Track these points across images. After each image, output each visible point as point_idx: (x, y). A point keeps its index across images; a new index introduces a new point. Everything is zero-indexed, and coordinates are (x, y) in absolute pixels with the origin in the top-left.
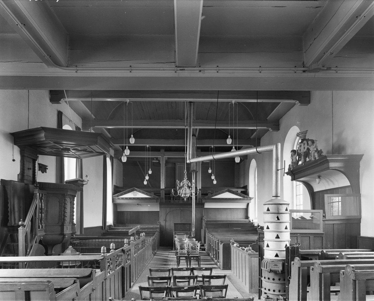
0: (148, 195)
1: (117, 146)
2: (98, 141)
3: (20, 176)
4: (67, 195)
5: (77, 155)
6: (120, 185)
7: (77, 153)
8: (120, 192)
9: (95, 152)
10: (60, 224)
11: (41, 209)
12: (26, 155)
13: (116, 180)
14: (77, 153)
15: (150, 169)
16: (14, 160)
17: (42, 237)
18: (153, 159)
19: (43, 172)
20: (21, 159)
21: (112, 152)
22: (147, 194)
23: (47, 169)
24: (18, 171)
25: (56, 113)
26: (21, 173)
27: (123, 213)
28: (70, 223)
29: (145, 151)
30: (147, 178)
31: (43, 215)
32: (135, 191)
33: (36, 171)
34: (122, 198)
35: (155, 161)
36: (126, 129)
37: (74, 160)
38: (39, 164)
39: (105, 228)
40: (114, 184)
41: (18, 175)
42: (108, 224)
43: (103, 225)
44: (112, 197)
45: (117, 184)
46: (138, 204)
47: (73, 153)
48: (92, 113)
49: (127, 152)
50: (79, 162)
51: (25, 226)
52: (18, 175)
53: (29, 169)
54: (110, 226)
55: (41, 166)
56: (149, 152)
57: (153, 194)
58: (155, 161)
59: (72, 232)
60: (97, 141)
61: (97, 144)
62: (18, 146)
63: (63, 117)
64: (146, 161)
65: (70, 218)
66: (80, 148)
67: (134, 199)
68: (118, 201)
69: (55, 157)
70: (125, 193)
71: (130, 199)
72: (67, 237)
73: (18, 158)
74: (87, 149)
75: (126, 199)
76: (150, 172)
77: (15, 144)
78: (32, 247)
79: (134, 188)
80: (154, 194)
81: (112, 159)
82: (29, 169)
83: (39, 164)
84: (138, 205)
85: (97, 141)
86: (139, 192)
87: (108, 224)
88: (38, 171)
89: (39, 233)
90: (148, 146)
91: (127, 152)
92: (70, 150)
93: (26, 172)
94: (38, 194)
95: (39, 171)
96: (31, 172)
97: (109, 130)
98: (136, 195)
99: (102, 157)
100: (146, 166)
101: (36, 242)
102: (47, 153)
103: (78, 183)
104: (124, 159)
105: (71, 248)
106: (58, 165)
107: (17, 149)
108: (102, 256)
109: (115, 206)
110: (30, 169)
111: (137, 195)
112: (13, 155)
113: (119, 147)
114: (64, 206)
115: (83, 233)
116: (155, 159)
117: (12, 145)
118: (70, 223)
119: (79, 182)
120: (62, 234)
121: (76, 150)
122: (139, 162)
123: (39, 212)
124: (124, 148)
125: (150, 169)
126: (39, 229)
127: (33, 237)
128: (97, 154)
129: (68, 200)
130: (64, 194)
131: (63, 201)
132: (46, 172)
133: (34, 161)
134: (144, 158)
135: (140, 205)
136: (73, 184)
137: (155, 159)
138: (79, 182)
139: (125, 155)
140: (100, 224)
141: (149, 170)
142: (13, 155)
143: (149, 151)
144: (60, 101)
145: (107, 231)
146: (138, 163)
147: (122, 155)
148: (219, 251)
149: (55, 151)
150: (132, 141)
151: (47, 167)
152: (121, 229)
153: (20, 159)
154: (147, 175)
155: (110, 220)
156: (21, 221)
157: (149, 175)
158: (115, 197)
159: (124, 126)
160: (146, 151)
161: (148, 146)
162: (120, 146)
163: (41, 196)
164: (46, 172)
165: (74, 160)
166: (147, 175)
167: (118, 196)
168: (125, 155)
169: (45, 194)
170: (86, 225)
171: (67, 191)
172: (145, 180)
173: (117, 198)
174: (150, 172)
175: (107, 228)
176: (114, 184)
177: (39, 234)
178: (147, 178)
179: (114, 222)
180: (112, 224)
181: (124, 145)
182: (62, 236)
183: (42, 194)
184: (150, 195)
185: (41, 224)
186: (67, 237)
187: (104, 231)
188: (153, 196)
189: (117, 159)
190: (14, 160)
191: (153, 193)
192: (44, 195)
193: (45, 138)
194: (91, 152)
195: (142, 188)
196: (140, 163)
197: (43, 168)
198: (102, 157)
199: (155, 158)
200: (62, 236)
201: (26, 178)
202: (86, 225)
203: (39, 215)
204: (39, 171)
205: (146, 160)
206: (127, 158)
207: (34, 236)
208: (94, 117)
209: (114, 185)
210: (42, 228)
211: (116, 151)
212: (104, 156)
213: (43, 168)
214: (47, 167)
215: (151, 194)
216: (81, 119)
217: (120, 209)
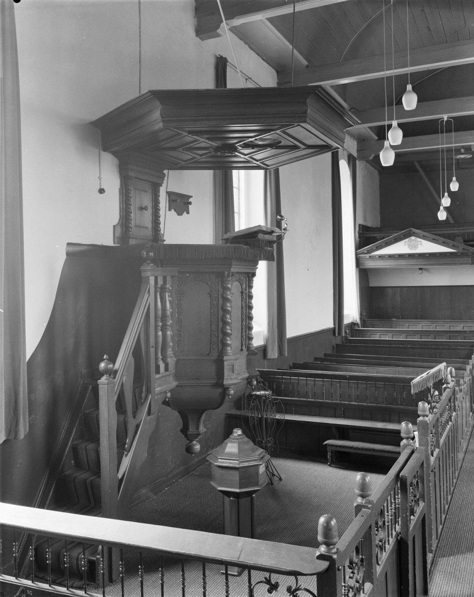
0: (448, 247)
1: (363, 128)
2: (309, 111)
3: (119, 230)
4: (228, 276)
5: (257, 161)
6: (373, 221)
7: (258, 156)
8: (374, 240)
9: (302, 146)
10: (215, 355)
11: (164, 316)
12: (131, 174)
13: (365, 211)
14: (258, 156)
15: (454, 179)
16: (102, 191)
17: (169, 395)
18: (458, 151)
19: (180, 214)
20: (121, 185)
21: (351, 145)
22: (444, 244)
23: (190, 203)
24: (114, 216)
25: (212, 62)
26: (122, 223)
27: (382, 290)
28: (242, 350)
29: (439, 133)
30: (446, 202)
31: (169, 333)
32: (413, 238)
33: (162, 213)
34: (381, 257)
35: (462, 156)
36: (389, 78)
37: (258, 175)
38: (169, 194)
39: (340, 333)
40: (360, 221)
41: (114, 226)
42: (347, 321)
43: (334, 324)
44: (356, 254)
45: (365, 220)
46: (421, 269)
47: (246, 157)
48: (295, 46)
49: (395, 137)
50: (270, 178)
51: (116, 372)
52: (114, 226)
53: (141, 209)
54: (353, 325)
55: (174, 198)
56: (449, 134)
57: (462, 240)
58: (462, 156)
59: (248, 375)
60: (307, 111)
61: (305, 122)
62: (115, 154)
63: (229, 70)
64: (443, 160)
65: (242, 337)
66: (261, 139)
67: (411, 256)
68: (370, 264)
69: (211, 172)
70: (388, 244)
71: (401, 256)
72: (232, 392)
73: (112, 182)
74: (280, 142)
75: (391, 257)
76: (454, 186)
77: (105, 150)
78: (138, 426)
79: (411, 230)
80: (465, 241)
81: (351, 160)
82: (141, 209)
83: (169, 194)
84: (420, 271)
85: (306, 112)
86: (424, 238)
87: (347, 321)
88: (168, 212)
89: (160, 385)
90: (445, 117)
91: (395, 137)
92: (235, 149)
93: (135, 217)
94: (152, 280)
95: (170, 210)
96: (148, 215)
97: (342, 89)
98: (416, 247)
99: (328, 156)
100: (443, 170)
101: (149, 413)
102: (184, 163)
103: (259, 240)
104: (387, 159)
105: (239, 435)
106: (217, 190)
107: (109, 163)
108: (321, 557)
109: (364, 274)
110: (146, 208)
111: (419, 246)
112: (100, 178)
113: (368, 129)
114: (223, 305)
115: (286, 355)
116: (463, 151)
117: (97, 151)
118: (242, 350)
119: (260, 236)
120: (219, 383)
121: (253, 148)
122: (419, 162)
123: (156, 326)
124: (382, 133)
125: (454, 179)
126: (157, 376)
127: (141, 398)
128: (311, 150)
129: (234, 288)
130: (223, 273)
131: (220, 293)
132: (188, 213)
133: (155, 189)
134: (436, 151)
135: (426, 270)
136: (247, 244)
137: (463, 151)
138: (260, 236)
139: (390, 145)
140: (328, 323)
141: (450, 181)
142: (100, 178)
143: (449, 131)
144: (218, 29)
145: (346, 338)
146: (417, 165)
147: (382, 147)
148: (300, 112)
149: (201, 155)
150: (410, 101)
151: (190, 200)
152: (380, 334)
153: (118, 186)
154: (446, 194)
155: (352, 311)
156: (104, 360)
157: (452, 195)
158: (363, 253)
159: (383, 70)
160: (442, 132)
161: (445, 117)
162: (370, 128)
163: (160, 282)
164: (188, 213)
165: (258, 175)
166: (446, 194)
167: (369, 252)
168: (390, 145)
169: (172, 277)
170: (291, 332)
171: (231, 265)
172: (441, 208)
173: (367, 256)
174: (454, 186)
175: (346, 332)
176: (360, 221)
177: (158, 389)
178: (446, 202)
179: (361, 314)
180: (358, 321)
181: (386, 123)
182: (220, 390)
183: (165, 278)
184: (453, 247)
185: (164, 360)
186: (232, 392)
187: (338, 340)
188: (462, 246)
189: (365, 162)
190: (102, 191)
191: (461, 239)
192: (169, 279)
193: (163, 121)
194: (294, 148)
195: (433, 230)
196: (422, 166)
197: (180, 203)
198: (328, 156)
199: (463, 147)
200: (220, 390)
201: (134, 231)
202: (291, 332)
203: (156, 336)
204: (170, 210)
205: (443, 155)
206: (397, 156)
207: (143, 395)
208: (305, 63)
209: (359, 225)
210: (166, 369)
211: (362, 140)
212: (333, 153)
213: (180, 203)
214: (190, 200)
215: (455, 243)
216: (274, 72)
217: (374, 283)
